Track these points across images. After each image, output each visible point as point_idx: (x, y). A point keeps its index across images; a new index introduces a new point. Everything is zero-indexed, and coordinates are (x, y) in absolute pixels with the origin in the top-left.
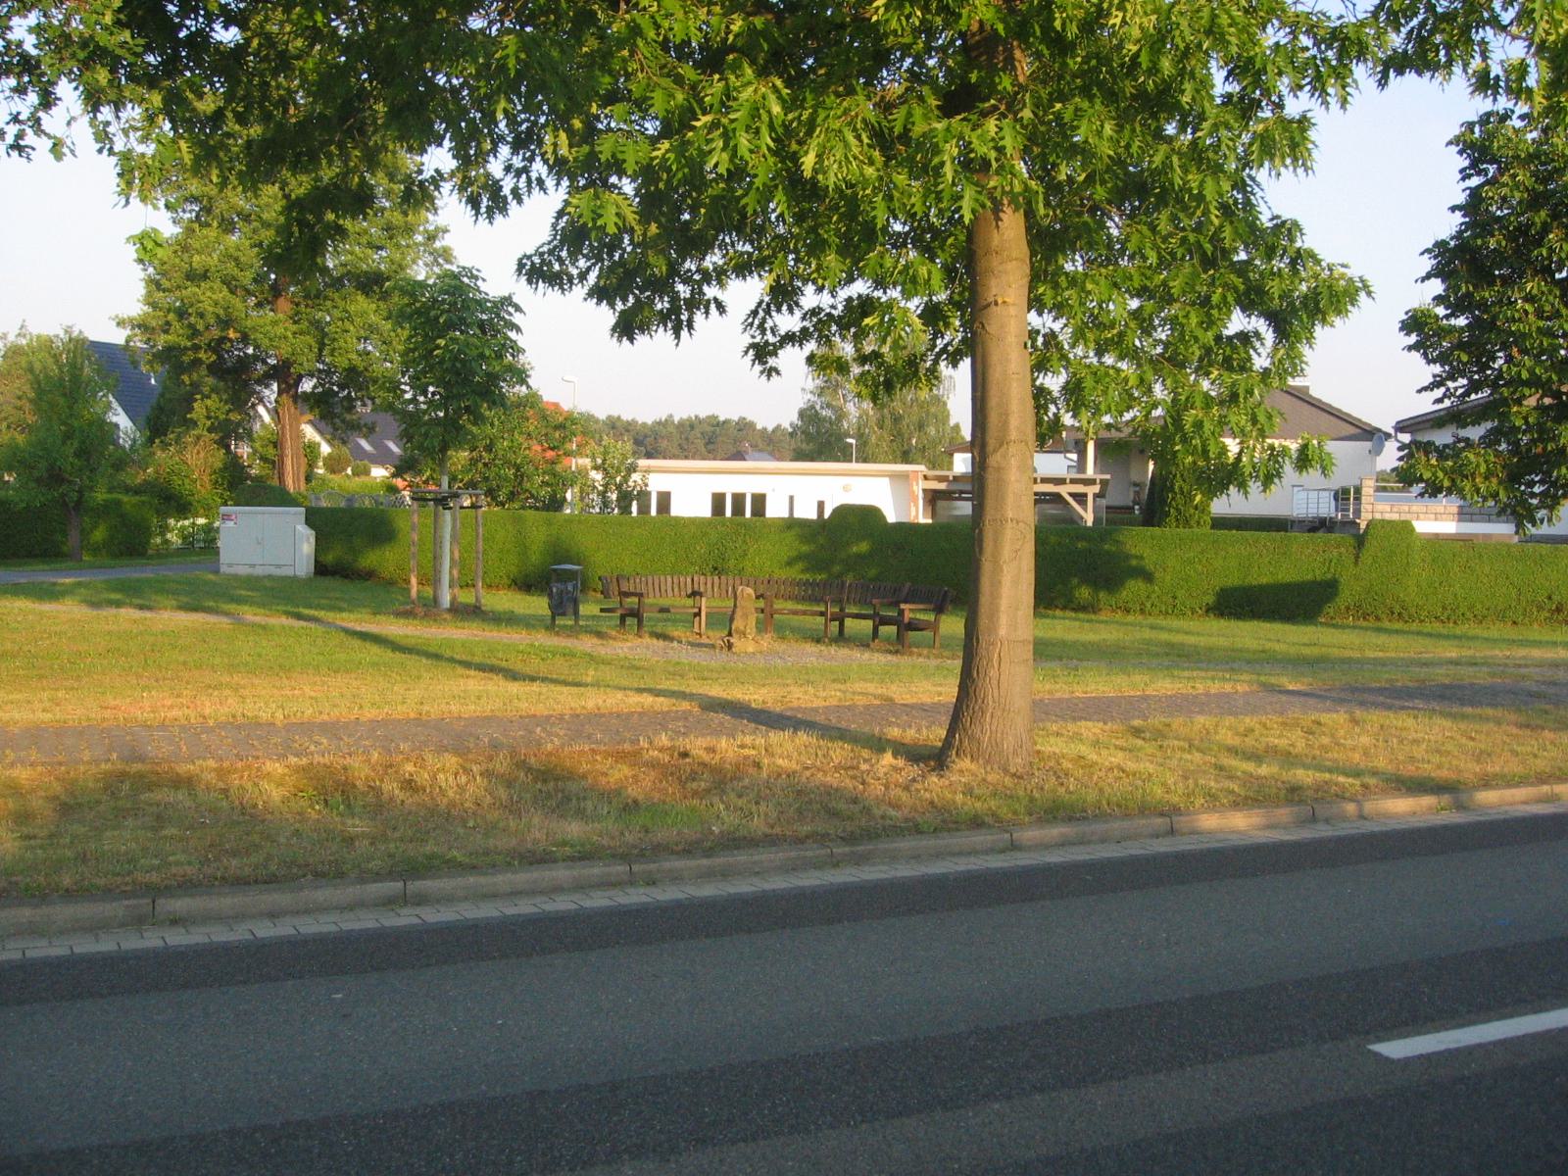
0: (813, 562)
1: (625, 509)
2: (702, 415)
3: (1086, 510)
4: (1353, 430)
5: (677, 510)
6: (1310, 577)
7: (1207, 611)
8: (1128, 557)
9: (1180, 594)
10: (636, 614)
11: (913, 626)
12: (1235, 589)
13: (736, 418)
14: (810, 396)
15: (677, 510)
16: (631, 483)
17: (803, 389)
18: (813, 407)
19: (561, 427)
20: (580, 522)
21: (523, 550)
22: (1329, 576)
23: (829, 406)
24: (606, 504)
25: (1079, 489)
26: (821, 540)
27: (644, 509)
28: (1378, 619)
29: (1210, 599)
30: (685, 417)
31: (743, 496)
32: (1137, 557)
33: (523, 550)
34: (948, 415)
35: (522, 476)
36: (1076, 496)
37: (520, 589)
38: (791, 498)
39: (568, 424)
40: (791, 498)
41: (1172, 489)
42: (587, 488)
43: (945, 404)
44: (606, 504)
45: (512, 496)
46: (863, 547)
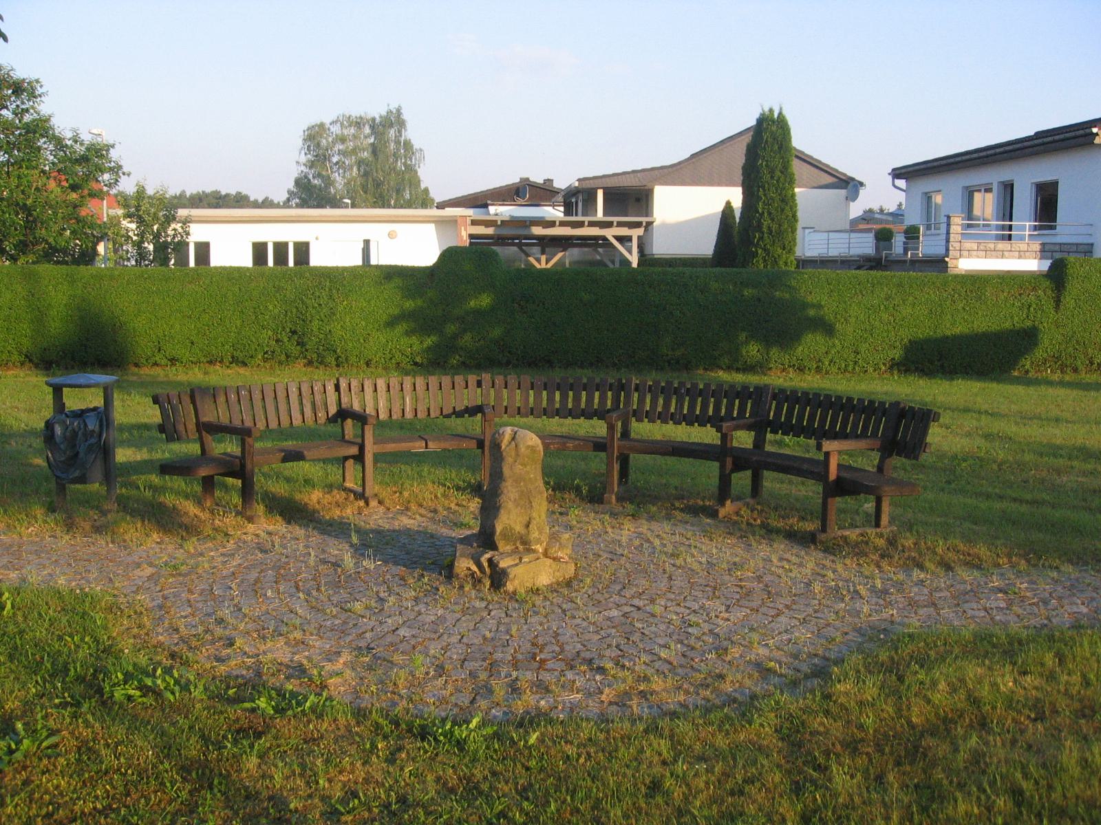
0: (420, 323)
1: (165, 262)
2: (208, 190)
3: (630, 252)
4: (830, 180)
5: (218, 259)
6: (1007, 325)
7: (891, 368)
8: (805, 306)
9: (863, 347)
10: (239, 469)
11: (845, 486)
12: (928, 341)
13: (234, 193)
14: (303, 168)
15: (218, 259)
16: (170, 232)
17: (298, 162)
18: (306, 177)
19: (84, 159)
20: (112, 278)
21: (39, 319)
22: (1029, 323)
23: (319, 175)
24: (142, 255)
25: (624, 231)
26: (430, 294)
27: (183, 261)
28: (1075, 370)
29: (897, 354)
30: (195, 192)
31: (286, 244)
32: (813, 306)
33: (39, 319)
34: (419, 181)
35: (34, 221)
36: (621, 239)
37: (37, 366)
38: (367, 242)
39: (91, 155)
40: (367, 242)
41: (760, 226)
42: (118, 240)
43: (416, 172)
44: (142, 255)
45: (23, 247)
46: (485, 301)
